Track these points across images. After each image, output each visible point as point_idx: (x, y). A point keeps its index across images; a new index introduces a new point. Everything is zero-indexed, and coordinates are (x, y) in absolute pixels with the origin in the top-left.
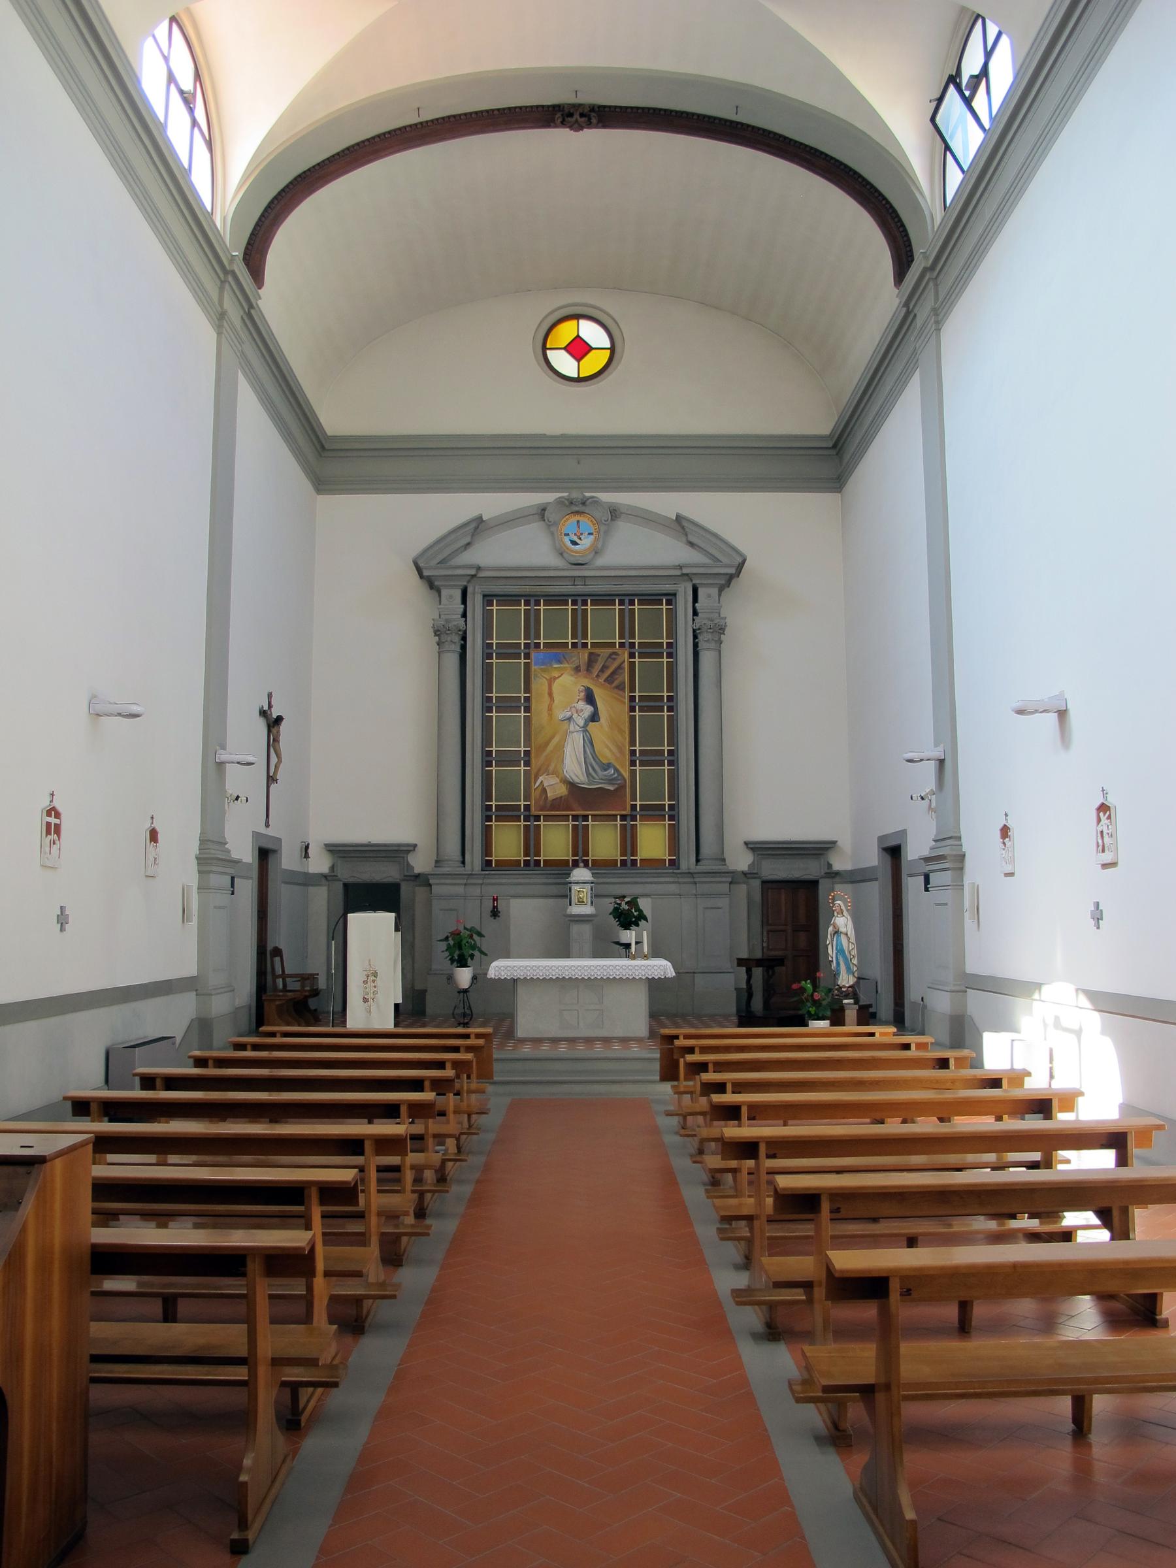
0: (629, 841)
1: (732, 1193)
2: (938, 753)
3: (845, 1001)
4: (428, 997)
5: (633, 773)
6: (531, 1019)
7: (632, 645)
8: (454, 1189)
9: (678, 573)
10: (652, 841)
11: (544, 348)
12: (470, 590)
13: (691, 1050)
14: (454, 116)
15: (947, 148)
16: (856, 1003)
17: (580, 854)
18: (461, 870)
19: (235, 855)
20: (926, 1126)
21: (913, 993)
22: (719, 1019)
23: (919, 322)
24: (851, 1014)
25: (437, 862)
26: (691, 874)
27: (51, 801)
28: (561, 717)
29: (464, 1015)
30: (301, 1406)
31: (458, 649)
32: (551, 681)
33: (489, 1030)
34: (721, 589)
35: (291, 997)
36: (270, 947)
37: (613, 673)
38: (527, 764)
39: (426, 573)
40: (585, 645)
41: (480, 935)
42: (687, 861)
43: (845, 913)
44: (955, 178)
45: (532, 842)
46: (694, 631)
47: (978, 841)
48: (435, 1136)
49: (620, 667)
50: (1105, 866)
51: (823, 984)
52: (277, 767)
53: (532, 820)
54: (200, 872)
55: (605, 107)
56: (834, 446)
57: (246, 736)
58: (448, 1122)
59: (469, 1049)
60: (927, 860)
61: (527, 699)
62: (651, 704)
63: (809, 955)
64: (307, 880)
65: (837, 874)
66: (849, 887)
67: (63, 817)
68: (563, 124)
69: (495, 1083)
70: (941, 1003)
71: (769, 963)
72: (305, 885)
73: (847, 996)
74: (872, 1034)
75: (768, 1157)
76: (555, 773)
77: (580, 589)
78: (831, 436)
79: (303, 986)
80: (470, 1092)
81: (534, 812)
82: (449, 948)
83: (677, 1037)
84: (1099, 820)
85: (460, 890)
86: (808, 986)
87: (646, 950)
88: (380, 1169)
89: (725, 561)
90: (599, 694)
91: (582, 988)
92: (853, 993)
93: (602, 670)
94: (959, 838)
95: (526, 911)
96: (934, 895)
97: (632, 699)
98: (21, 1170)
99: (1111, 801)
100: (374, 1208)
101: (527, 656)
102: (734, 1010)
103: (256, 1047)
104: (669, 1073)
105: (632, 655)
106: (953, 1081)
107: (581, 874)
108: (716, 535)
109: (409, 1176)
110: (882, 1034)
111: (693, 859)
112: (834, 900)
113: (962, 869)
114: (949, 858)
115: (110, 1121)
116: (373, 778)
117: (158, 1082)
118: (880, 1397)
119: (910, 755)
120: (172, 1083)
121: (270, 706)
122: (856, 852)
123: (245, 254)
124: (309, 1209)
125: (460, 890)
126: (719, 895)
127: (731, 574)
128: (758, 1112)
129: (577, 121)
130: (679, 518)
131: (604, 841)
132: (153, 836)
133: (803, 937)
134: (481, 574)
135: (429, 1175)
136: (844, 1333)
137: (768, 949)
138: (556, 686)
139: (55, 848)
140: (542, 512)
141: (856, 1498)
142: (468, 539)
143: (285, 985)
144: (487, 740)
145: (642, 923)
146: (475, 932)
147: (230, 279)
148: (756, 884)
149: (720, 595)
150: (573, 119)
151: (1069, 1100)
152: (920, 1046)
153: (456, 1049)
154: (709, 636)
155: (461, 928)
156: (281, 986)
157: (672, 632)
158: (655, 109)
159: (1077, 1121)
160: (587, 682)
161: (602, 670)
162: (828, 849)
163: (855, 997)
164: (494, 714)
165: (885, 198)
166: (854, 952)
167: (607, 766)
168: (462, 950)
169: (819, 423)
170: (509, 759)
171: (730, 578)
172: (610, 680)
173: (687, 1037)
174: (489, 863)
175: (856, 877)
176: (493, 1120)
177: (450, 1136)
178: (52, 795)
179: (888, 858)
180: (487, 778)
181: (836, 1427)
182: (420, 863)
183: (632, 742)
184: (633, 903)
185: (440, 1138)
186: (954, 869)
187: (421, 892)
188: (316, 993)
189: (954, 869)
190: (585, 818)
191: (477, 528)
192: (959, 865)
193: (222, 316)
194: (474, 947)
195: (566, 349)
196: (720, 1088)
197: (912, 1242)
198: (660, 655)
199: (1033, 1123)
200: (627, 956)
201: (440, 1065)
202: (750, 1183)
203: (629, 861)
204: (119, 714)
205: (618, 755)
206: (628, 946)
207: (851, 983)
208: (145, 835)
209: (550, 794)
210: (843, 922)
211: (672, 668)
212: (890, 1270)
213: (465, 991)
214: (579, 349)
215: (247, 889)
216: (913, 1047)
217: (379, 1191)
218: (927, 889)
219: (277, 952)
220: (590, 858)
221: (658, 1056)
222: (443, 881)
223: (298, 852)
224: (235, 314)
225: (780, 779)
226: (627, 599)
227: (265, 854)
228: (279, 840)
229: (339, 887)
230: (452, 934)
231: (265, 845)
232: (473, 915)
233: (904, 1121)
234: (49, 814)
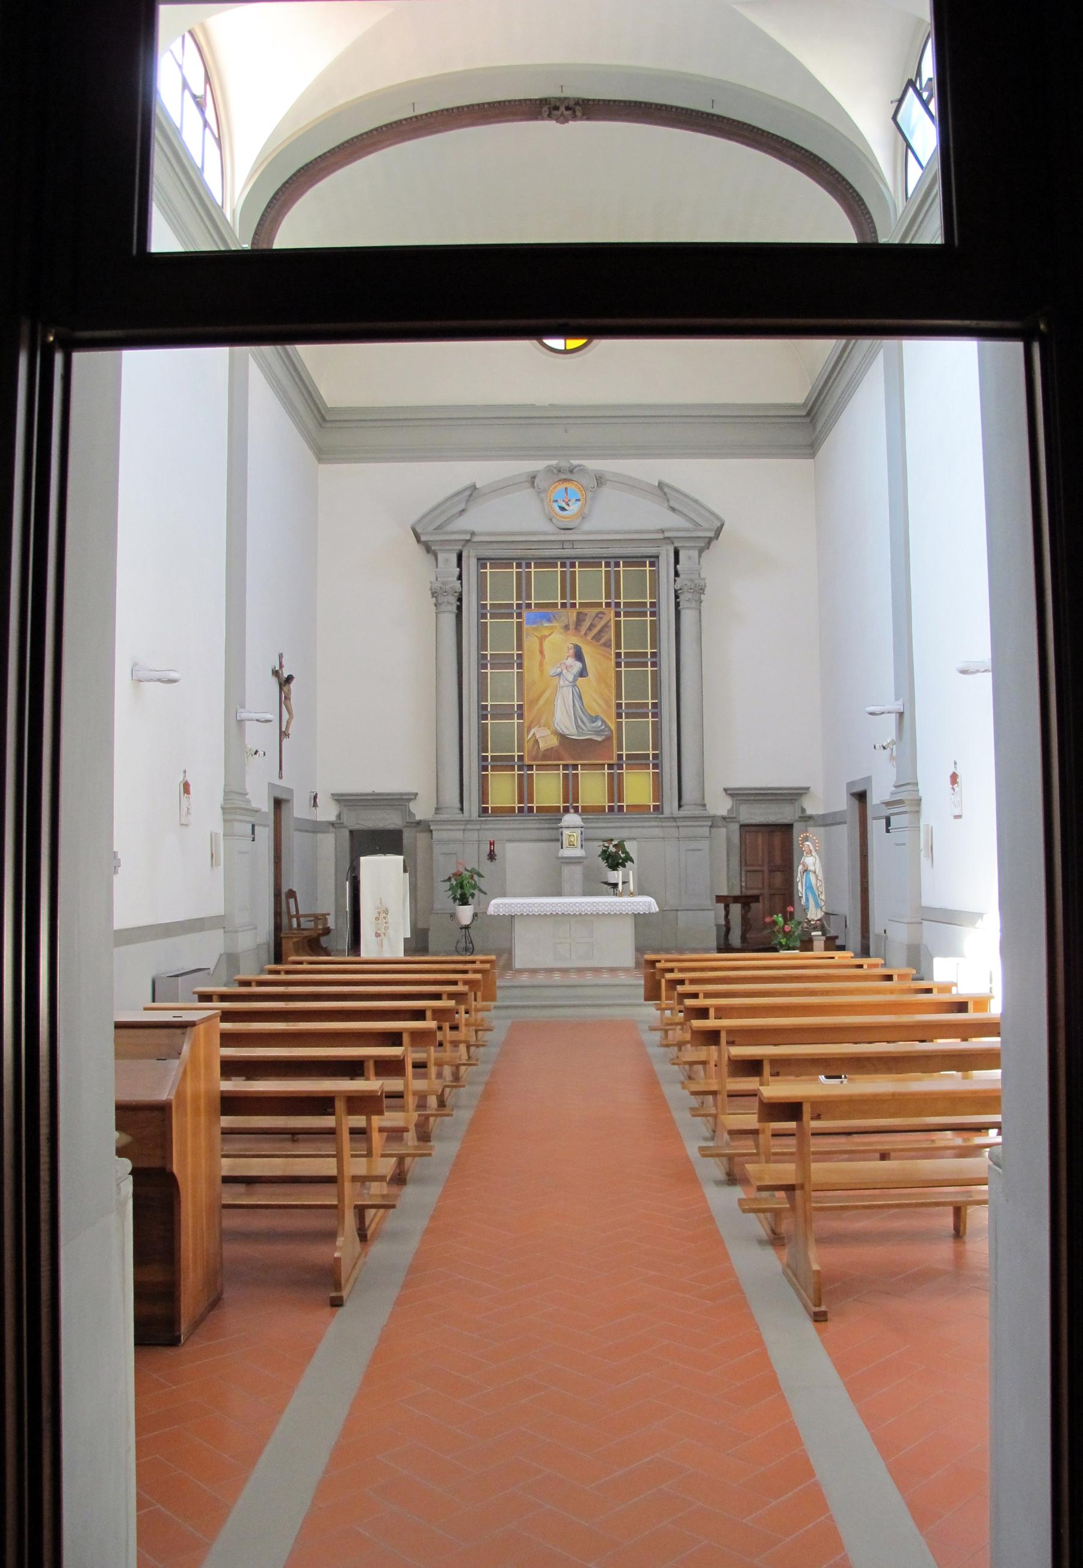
0: (616, 789)
2: (898, 706)
3: (813, 934)
4: (430, 933)
5: (619, 725)
6: (527, 952)
7: (618, 605)
9: (661, 536)
10: (638, 787)
12: (464, 554)
14: (447, 110)
15: (908, 146)
16: (823, 935)
17: (571, 800)
18: (459, 817)
19: (254, 805)
21: (877, 926)
24: (819, 943)
25: (437, 809)
26: (674, 819)
30: (367, 1223)
32: (542, 639)
34: (701, 551)
35: (299, 937)
36: (284, 890)
37: (601, 631)
38: (521, 716)
39: (423, 538)
40: (573, 605)
41: (480, 875)
42: (670, 806)
43: (814, 853)
45: (525, 790)
46: (676, 591)
48: (355, 1179)
49: (606, 626)
52: (288, 723)
54: (225, 821)
55: (589, 100)
56: (808, 414)
57: (261, 692)
58: (445, 1051)
60: (888, 804)
61: (520, 656)
62: (636, 660)
63: (785, 895)
64: (316, 828)
65: (810, 817)
66: (822, 830)
68: (550, 117)
71: (746, 901)
72: (314, 832)
73: (815, 929)
76: (547, 725)
78: (804, 405)
79: (316, 925)
80: (477, 1010)
81: (527, 762)
85: (459, 835)
86: (780, 919)
87: (632, 888)
89: (705, 525)
91: (573, 926)
93: (589, 629)
94: (916, 784)
95: (521, 853)
97: (618, 655)
98: (178, 1031)
105: (618, 614)
107: (571, 819)
108: (696, 501)
109: (411, 1101)
112: (806, 839)
113: (918, 812)
118: (798, 1193)
121: (281, 666)
122: (827, 798)
125: (459, 835)
126: (696, 838)
129: (562, 114)
130: (661, 486)
131: (593, 788)
133: (778, 879)
134: (476, 539)
135: (433, 1101)
136: (780, 1157)
137: (746, 888)
138: (546, 645)
140: (532, 479)
141: (784, 1272)
142: (462, 506)
143: (299, 924)
144: (482, 694)
145: (628, 864)
146: (474, 873)
148: (735, 827)
149: (700, 557)
150: (559, 113)
154: (690, 596)
155: (461, 869)
156: (295, 925)
158: (635, 102)
160: (576, 640)
161: (589, 629)
162: (801, 794)
164: (489, 671)
167: (594, 719)
170: (502, 713)
171: (710, 540)
172: (597, 638)
173: (667, 961)
174: (485, 810)
175: (828, 821)
176: (496, 1037)
179: (856, 803)
180: (483, 731)
181: (774, 1232)
182: (421, 810)
183: (619, 696)
184: (620, 846)
186: (911, 812)
187: (422, 837)
188: (327, 931)
189: (911, 812)
190: (575, 767)
191: (471, 495)
192: (916, 809)
194: (475, 887)
197: (884, 1156)
198: (644, 614)
200: (615, 895)
203: (616, 808)
204: (159, 680)
205: (604, 706)
206: (615, 885)
207: (819, 917)
208: (178, 788)
211: (655, 626)
212: (803, 1097)
213: (467, 927)
215: (265, 834)
218: (888, 831)
219: (292, 894)
220: (580, 805)
222: (449, 827)
223: (307, 801)
226: (613, 561)
228: (291, 791)
230: (455, 875)
232: (472, 858)
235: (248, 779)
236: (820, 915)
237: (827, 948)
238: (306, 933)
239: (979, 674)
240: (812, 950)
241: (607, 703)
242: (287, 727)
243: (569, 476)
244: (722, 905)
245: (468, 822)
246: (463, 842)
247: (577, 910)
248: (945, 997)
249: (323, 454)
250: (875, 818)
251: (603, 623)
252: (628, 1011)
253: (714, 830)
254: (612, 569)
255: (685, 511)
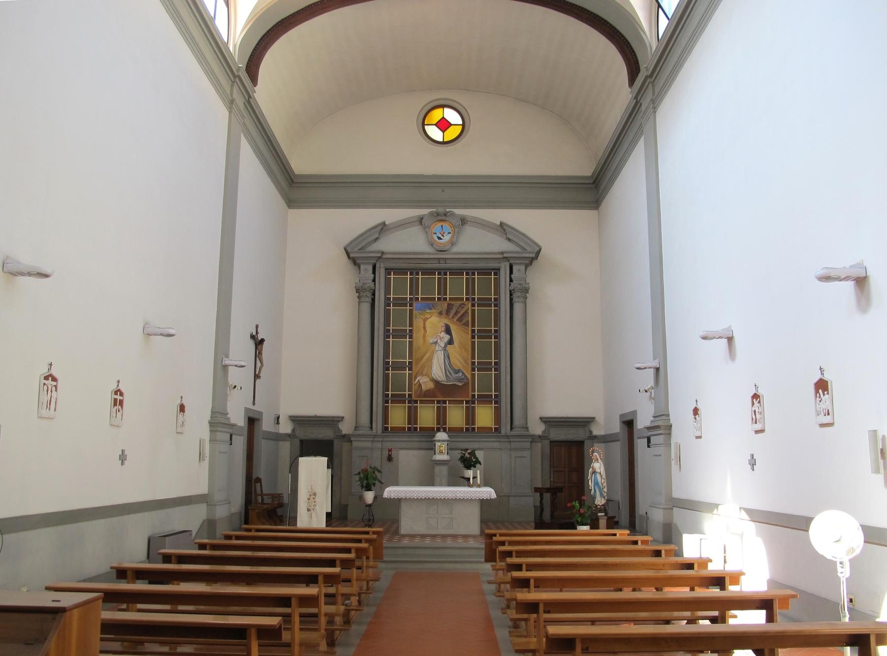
0: (470, 416)
1: (525, 633)
2: (655, 364)
5: (473, 375)
6: (409, 523)
7: (473, 299)
8: (354, 627)
9: (501, 256)
10: (484, 416)
11: (423, 125)
12: (377, 266)
13: (503, 543)
15: (659, 6)
18: (370, 432)
19: (233, 421)
20: (648, 593)
22: (523, 525)
23: (643, 108)
24: (603, 522)
26: (508, 437)
27: (49, 369)
28: (431, 341)
29: (369, 520)
31: (370, 300)
33: (381, 529)
34: (526, 267)
35: (265, 506)
36: (254, 477)
37: (463, 315)
38: (410, 369)
40: (445, 299)
42: (505, 429)
44: (663, 23)
45: (412, 416)
47: (680, 416)
48: (343, 595)
49: (466, 312)
50: (757, 432)
51: (587, 503)
52: (260, 369)
53: (412, 403)
54: (211, 431)
56: (594, 183)
57: (241, 350)
58: (352, 586)
59: (367, 541)
60: (649, 428)
61: (411, 331)
64: (278, 437)
65: (595, 437)
66: (602, 445)
67: (125, 395)
69: (385, 562)
70: (658, 516)
71: (554, 491)
73: (600, 511)
74: (615, 535)
75: (545, 612)
77: (442, 266)
79: (273, 501)
80: (368, 567)
81: (414, 398)
82: (360, 479)
83: (495, 535)
84: (753, 404)
85: (369, 444)
88: (301, 615)
89: (529, 249)
90: (454, 328)
91: (441, 504)
92: (604, 508)
93: (455, 314)
94: (668, 415)
95: (408, 458)
96: (653, 450)
97: (473, 331)
98: (49, 616)
99: (760, 392)
100: (297, 640)
101: (411, 305)
102: (532, 519)
103: (238, 538)
104: (490, 556)
105: (473, 305)
106: (664, 565)
107: (442, 436)
109: (323, 620)
110: (621, 535)
111: (509, 427)
112: (593, 452)
113: (670, 434)
114: (662, 427)
115: (150, 583)
116: (319, 376)
117: (173, 559)
119: (638, 365)
120: (182, 559)
121: (257, 333)
122: (607, 424)
123: (247, 66)
124: (250, 642)
125: (369, 444)
126: (523, 449)
127: (532, 257)
128: (541, 583)
130: (502, 224)
131: (456, 416)
132: (182, 408)
134: (385, 256)
135: (338, 620)
139: (119, 414)
140: (421, 220)
142: (376, 236)
143: (263, 500)
144: (386, 355)
145: (478, 465)
146: (375, 469)
147: (237, 80)
148: (547, 442)
151: (736, 578)
152: (643, 542)
153: (359, 541)
157: (497, 292)
159: (741, 591)
160: (446, 321)
161: (455, 314)
162: (589, 422)
163: (605, 511)
165: (623, 36)
166: (605, 484)
168: (369, 480)
169: (584, 168)
170: (400, 367)
172: (460, 320)
174: (386, 429)
175: (607, 439)
176: (384, 583)
177: (354, 595)
178: (51, 365)
179: (626, 428)
182: (346, 428)
183: (473, 357)
184: (472, 453)
185: (347, 596)
187: (346, 446)
188: (281, 505)
190: (445, 402)
191: (382, 229)
193: (232, 102)
194: (376, 479)
195: (436, 125)
196: (518, 567)
199: (714, 592)
201: (348, 550)
202: (535, 627)
203: (470, 428)
204: (161, 334)
206: (468, 479)
209: (424, 388)
210: (598, 466)
213: (370, 505)
214: (443, 125)
215: (240, 442)
216: (639, 543)
217: (301, 629)
218: (649, 446)
219: (258, 480)
221: (484, 546)
223: (272, 420)
224: (240, 101)
225: (561, 380)
227: (252, 421)
228: (261, 413)
229: (297, 442)
231: (252, 415)
233: (634, 590)
234: (116, 393)
235: (229, 404)
236: (603, 502)
237: (609, 527)
238: (265, 507)
239: (715, 340)
240: (598, 528)
241: (466, 361)
242: (260, 372)
243: (444, 218)
244: (538, 494)
245: (375, 436)
246: (372, 449)
247: (442, 496)
248: (703, 573)
249: (291, 203)
250: (639, 438)
251: (464, 310)
252: (475, 566)
253: (533, 444)
254: (470, 277)
255: (515, 240)
